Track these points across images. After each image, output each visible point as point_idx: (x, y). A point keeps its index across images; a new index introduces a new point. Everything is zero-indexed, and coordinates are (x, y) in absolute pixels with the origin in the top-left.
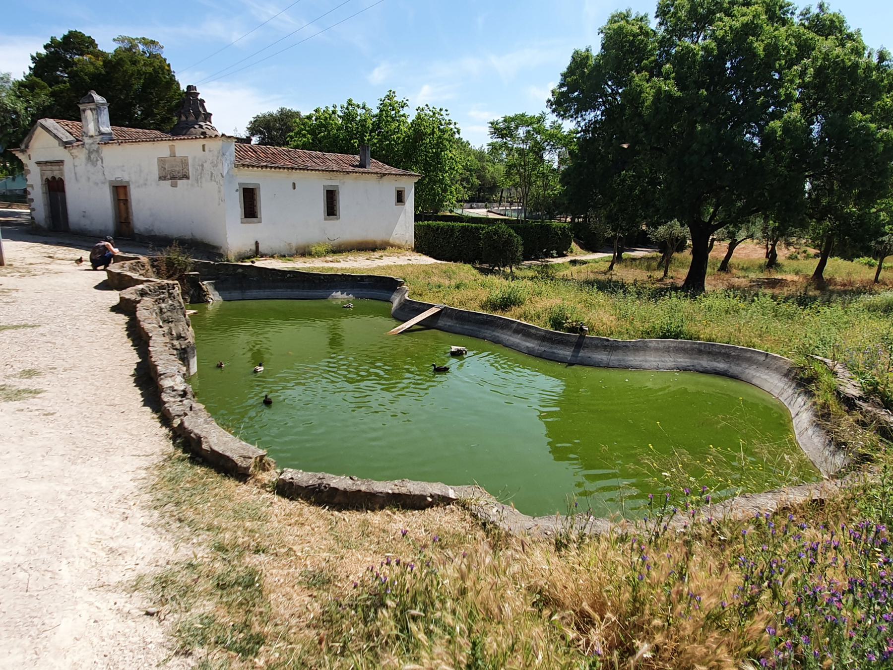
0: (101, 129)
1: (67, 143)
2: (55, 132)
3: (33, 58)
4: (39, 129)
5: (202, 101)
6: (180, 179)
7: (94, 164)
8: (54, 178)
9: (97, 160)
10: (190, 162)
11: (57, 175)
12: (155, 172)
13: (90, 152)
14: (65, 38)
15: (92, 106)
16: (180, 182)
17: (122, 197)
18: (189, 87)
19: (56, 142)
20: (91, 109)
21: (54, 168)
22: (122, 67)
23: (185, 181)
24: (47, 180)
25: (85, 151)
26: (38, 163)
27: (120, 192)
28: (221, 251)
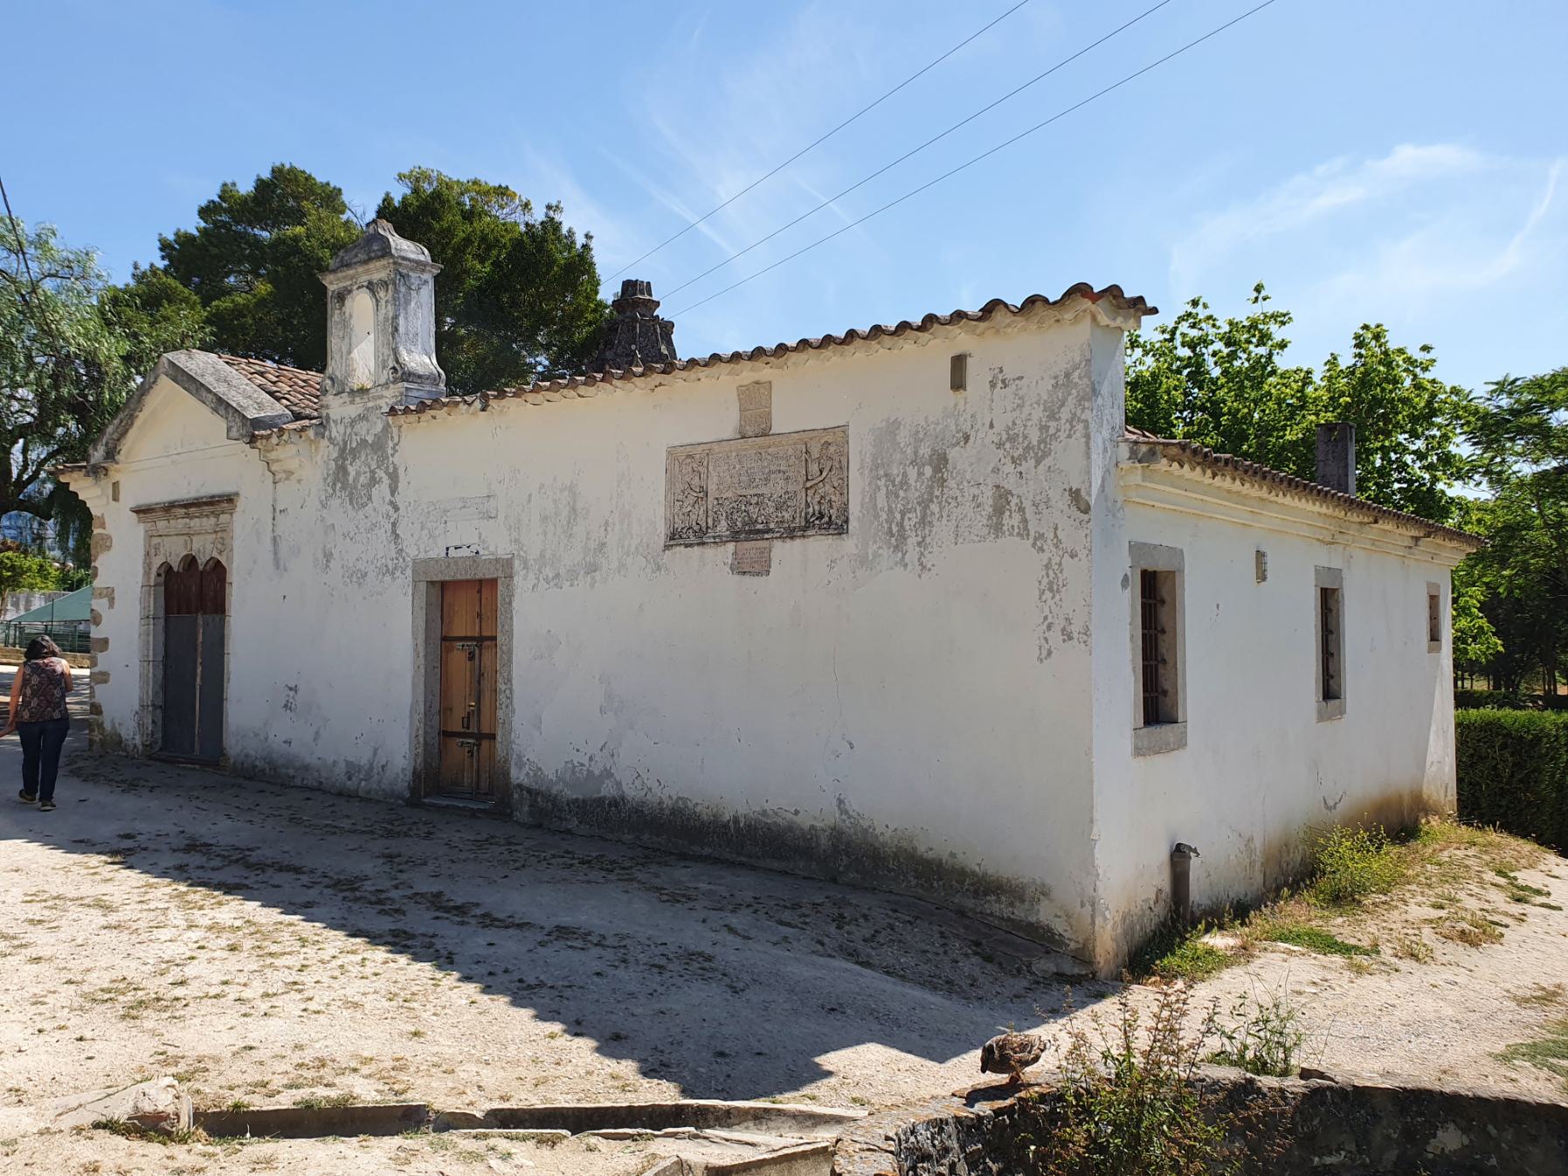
0: (405, 356)
1: (257, 423)
2: (220, 389)
3: (165, 246)
4: (165, 384)
5: (668, 327)
6: (791, 534)
7: (357, 497)
8: (190, 561)
9: (374, 481)
10: (859, 452)
11: (204, 548)
12: (652, 508)
13: (346, 453)
14: (261, 185)
15: (379, 271)
16: (784, 552)
17: (463, 626)
18: (630, 287)
19: (219, 424)
20: (371, 287)
21: (195, 523)
22: (440, 219)
23: (818, 545)
24: (167, 570)
25: (326, 451)
26: (142, 511)
27: (463, 616)
28: (1045, 914)
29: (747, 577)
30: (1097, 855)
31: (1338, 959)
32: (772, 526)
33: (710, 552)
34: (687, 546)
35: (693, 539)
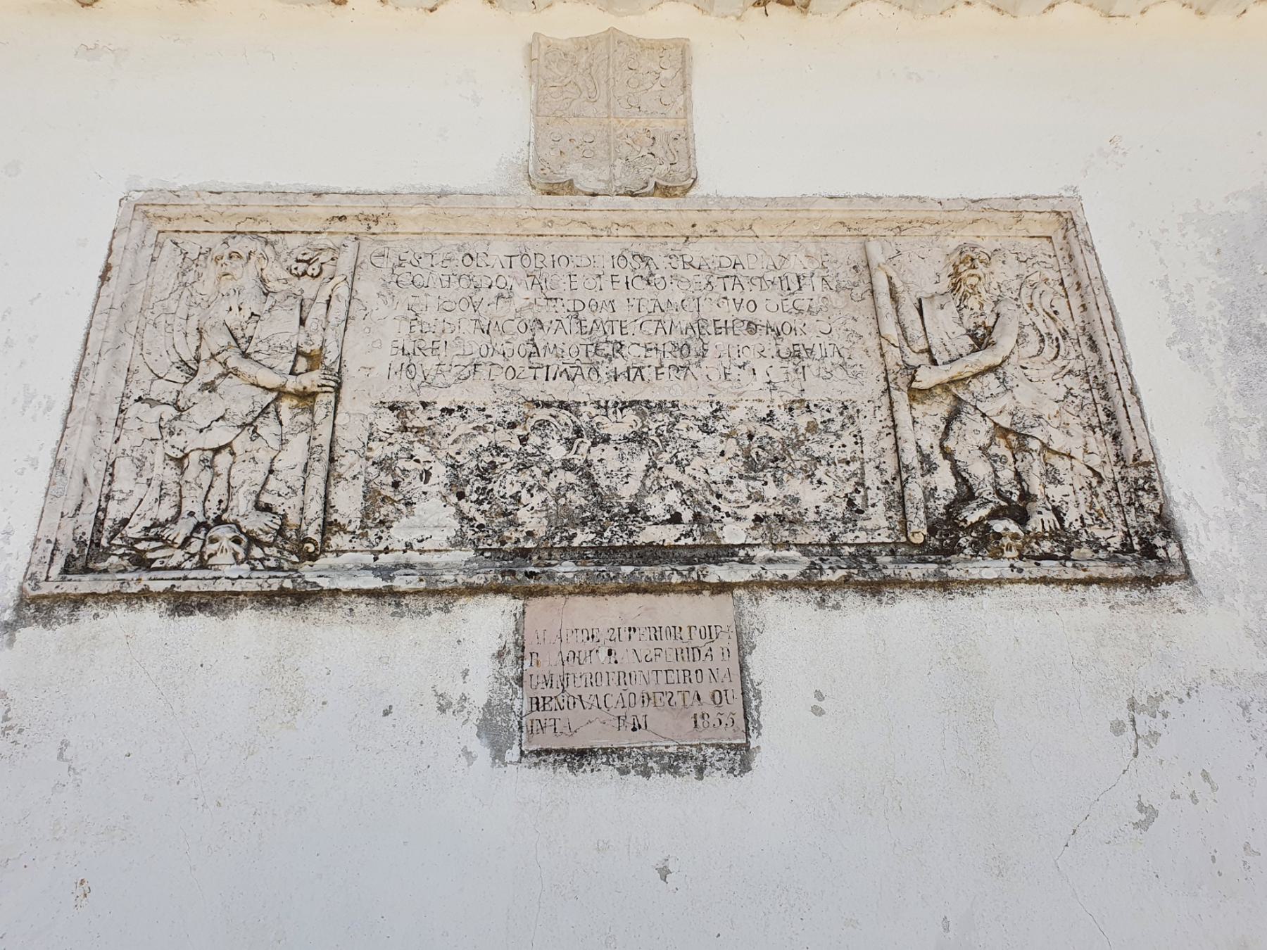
29: (600, 784)
30: (29, 629)
31: (748, 659)
32: (733, 533)
33: (337, 645)
34: (182, 604)
35: (228, 570)
